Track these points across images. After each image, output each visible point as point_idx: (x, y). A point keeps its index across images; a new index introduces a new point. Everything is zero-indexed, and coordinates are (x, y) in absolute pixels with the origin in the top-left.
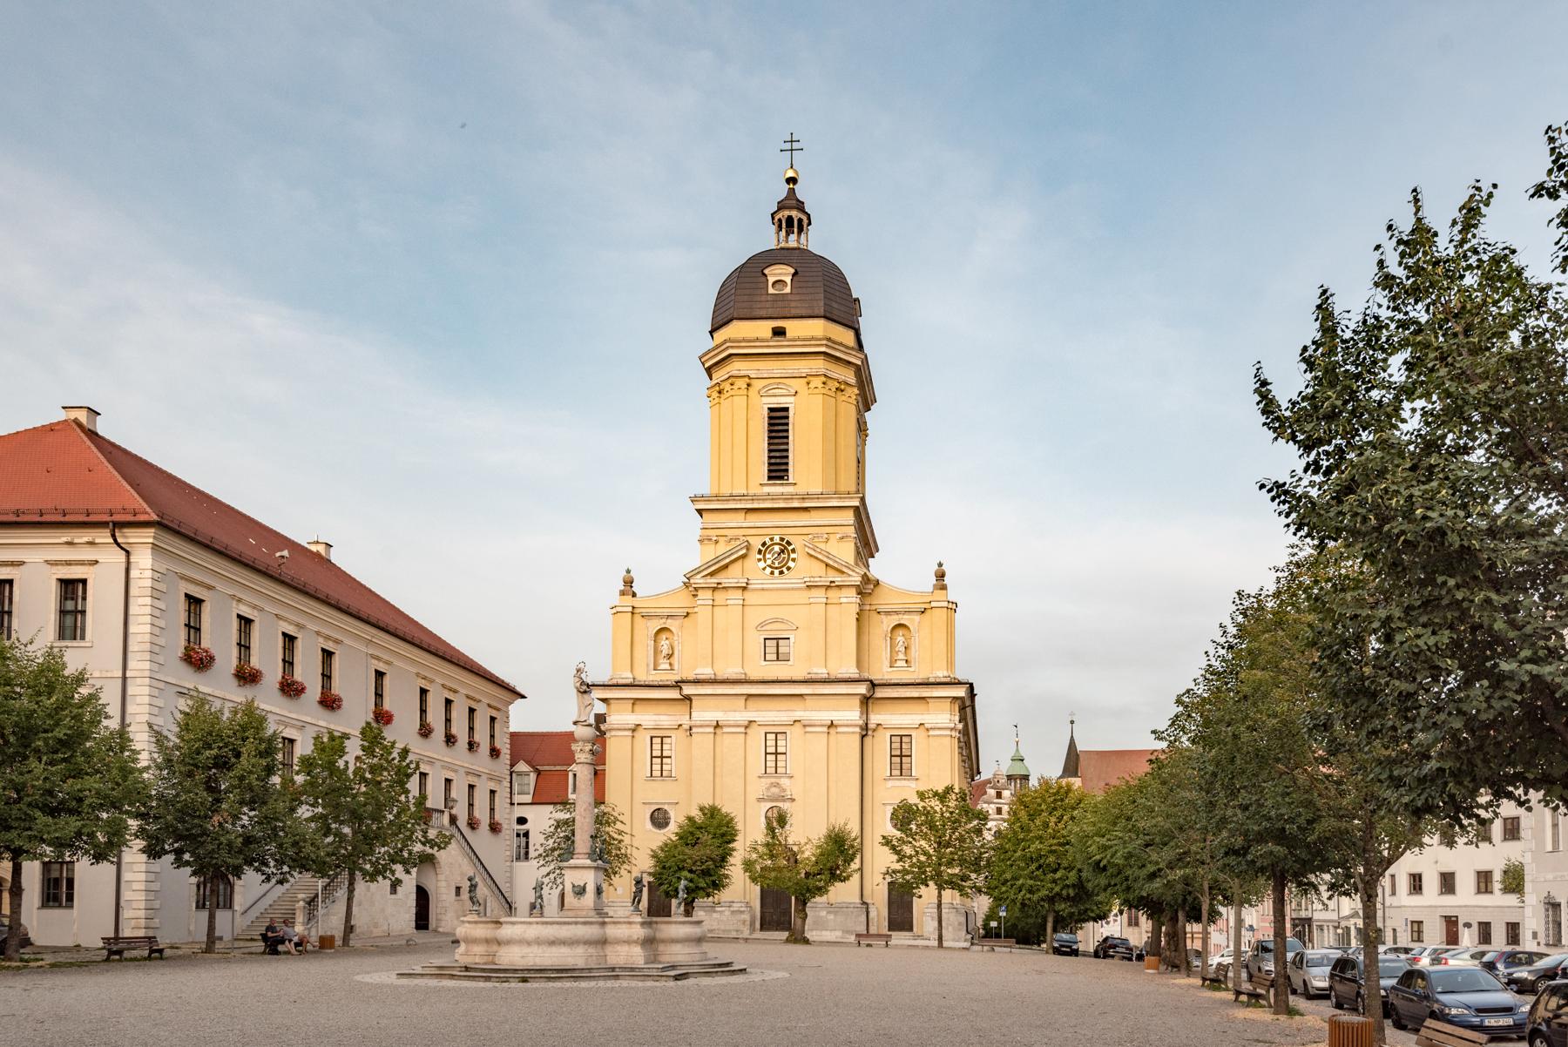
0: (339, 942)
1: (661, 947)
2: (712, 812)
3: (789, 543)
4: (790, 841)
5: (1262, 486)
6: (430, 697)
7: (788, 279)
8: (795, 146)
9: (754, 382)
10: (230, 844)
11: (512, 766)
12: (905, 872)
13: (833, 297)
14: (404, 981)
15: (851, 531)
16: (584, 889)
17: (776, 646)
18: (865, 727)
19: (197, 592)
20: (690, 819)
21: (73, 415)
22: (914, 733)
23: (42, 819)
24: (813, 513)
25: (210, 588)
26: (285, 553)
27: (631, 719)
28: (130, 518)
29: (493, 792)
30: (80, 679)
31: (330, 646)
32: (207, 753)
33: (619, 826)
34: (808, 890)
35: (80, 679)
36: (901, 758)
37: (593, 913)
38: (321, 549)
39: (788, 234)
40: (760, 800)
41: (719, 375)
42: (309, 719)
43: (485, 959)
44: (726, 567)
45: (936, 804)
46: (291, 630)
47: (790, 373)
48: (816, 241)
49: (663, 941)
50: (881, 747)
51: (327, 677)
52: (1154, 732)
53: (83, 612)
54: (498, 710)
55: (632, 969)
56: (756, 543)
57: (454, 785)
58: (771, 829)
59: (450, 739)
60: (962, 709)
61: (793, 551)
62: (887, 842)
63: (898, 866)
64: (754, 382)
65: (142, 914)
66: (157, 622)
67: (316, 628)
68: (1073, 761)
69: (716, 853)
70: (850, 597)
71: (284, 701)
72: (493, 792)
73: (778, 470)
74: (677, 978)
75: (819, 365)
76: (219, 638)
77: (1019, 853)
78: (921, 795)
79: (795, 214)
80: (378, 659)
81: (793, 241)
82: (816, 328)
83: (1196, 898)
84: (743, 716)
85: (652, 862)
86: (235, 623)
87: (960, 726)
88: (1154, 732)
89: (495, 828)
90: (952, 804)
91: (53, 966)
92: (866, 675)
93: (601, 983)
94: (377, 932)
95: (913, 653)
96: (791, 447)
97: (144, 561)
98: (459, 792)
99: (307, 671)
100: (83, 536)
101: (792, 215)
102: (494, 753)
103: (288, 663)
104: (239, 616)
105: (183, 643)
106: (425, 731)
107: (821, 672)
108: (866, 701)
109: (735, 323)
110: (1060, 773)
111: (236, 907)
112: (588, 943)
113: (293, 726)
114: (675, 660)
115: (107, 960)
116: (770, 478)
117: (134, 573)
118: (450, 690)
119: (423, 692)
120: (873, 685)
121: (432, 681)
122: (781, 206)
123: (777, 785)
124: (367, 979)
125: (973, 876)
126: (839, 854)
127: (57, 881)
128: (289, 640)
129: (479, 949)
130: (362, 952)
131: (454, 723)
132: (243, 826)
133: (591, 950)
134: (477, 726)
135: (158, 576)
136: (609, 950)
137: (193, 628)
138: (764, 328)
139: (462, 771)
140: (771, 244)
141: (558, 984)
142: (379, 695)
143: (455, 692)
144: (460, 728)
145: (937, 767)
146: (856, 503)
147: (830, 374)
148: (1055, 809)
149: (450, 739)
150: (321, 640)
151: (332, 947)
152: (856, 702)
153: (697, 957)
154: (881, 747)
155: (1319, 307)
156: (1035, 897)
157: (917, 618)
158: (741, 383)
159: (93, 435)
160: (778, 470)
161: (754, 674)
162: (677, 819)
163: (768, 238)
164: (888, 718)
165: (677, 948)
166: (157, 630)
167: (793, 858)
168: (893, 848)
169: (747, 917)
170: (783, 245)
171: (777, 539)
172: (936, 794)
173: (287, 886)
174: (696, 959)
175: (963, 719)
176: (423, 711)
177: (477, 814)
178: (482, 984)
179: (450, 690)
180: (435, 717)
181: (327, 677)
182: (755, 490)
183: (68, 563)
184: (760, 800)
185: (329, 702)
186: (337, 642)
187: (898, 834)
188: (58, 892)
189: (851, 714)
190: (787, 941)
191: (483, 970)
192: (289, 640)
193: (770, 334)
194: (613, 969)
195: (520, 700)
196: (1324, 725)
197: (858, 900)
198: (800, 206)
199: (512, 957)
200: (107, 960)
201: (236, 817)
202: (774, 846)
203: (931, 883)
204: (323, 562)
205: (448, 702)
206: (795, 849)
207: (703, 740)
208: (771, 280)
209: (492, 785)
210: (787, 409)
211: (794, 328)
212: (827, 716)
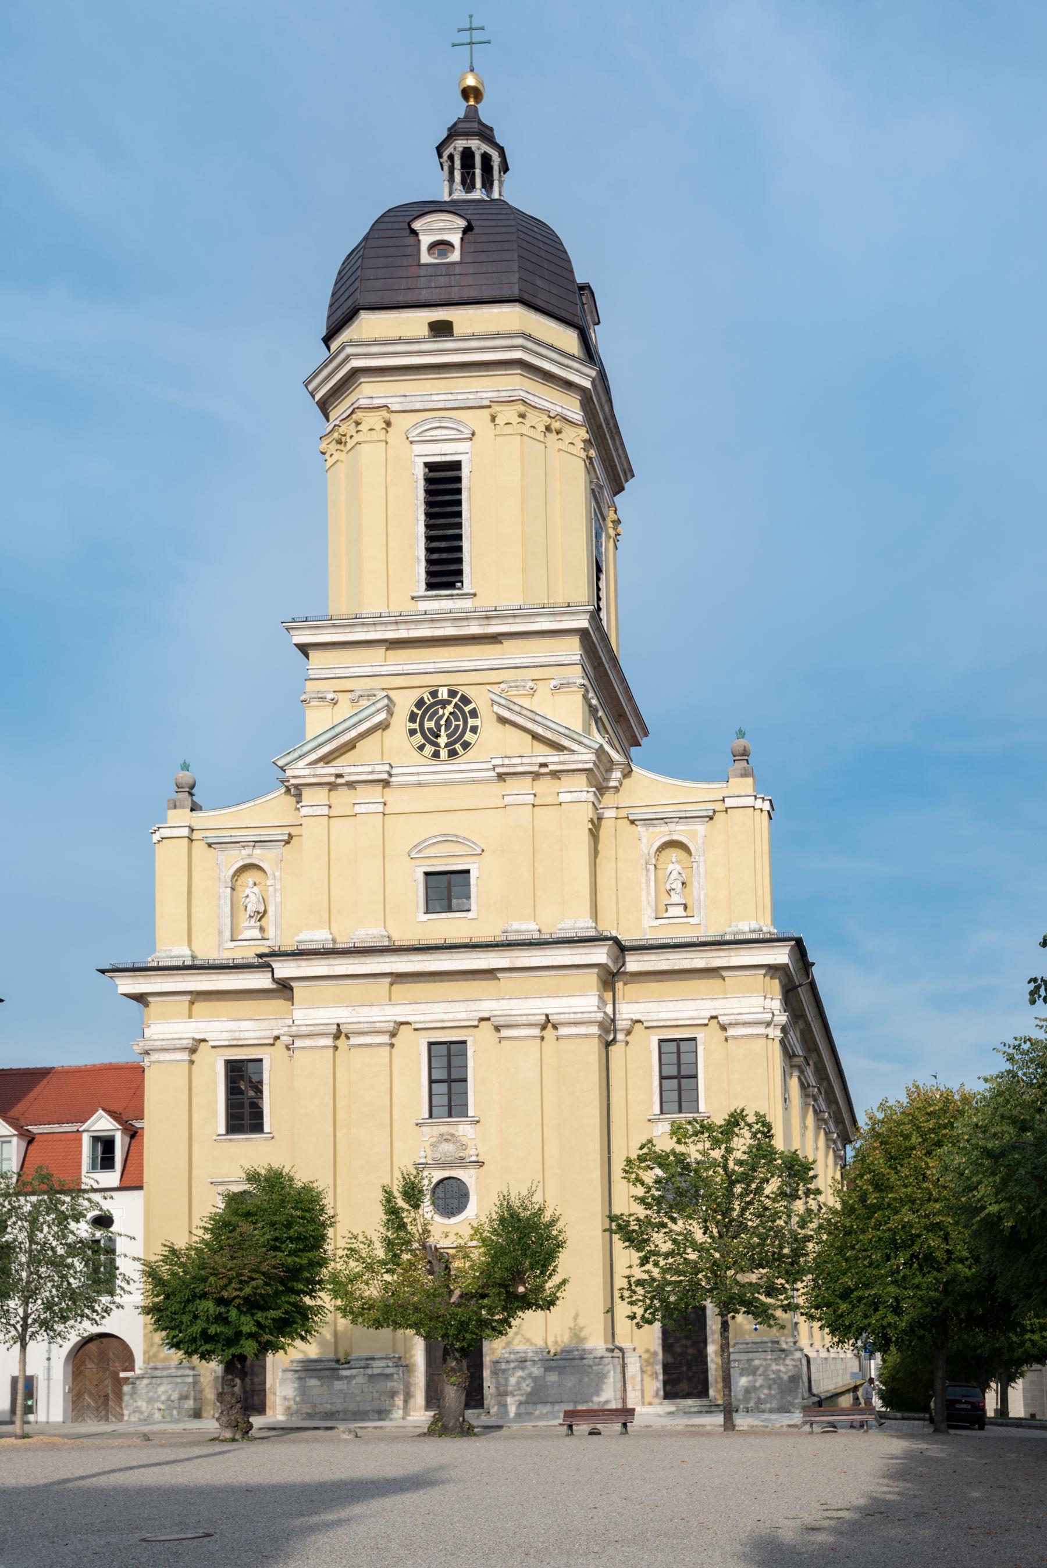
7: (455, 239)
8: (477, 36)
9: (394, 418)
13: (536, 270)
15: (577, 675)
17: (446, 889)
22: (700, 1035)
24: (507, 644)
36: (678, 1073)
47: (461, 399)
50: (640, 1066)
56: (405, 703)
61: (474, 714)
64: (394, 418)
70: (577, 792)
73: (444, 568)
75: (514, 383)
82: (511, 317)
84: (385, 1014)
95: (699, 891)
96: (466, 531)
107: (526, 927)
114: (269, 922)
116: (430, 586)
120: (621, 949)
126: (523, 1256)
138: (415, 322)
146: (583, 623)
148: (939, 1144)
152: (592, 978)
157: (700, 828)
160: (444, 568)
164: (634, 1005)
171: (443, 694)
182: (401, 604)
189: (582, 1001)
193: (425, 331)
198: (486, 134)
208: (426, 240)
210: (457, 465)
212: (537, 1007)
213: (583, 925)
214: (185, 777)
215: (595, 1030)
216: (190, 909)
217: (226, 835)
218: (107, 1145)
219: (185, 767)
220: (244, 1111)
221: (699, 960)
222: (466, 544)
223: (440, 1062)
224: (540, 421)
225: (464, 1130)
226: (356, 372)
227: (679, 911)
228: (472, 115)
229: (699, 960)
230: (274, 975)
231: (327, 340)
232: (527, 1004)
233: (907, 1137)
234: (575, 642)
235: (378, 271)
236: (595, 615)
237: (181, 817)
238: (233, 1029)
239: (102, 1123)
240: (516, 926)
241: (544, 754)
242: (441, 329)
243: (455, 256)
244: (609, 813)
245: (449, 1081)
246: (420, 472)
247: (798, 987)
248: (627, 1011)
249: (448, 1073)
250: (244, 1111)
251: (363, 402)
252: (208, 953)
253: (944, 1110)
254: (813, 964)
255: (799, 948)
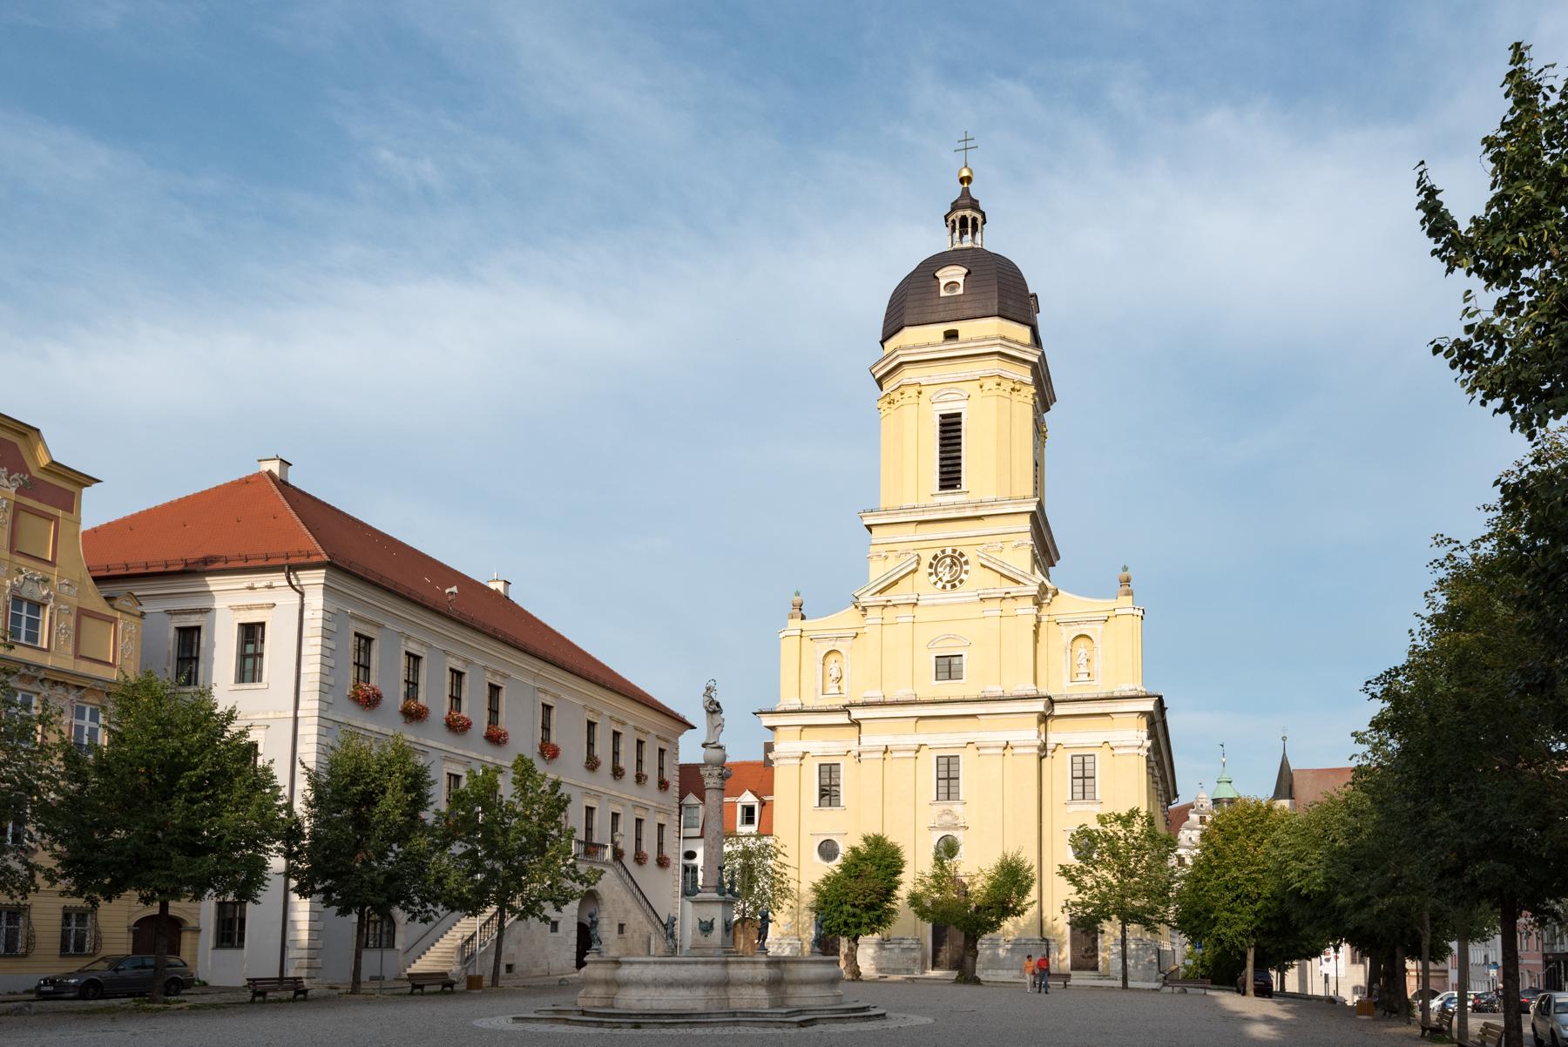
0: (487, 982)
1: (790, 990)
2: (877, 842)
3: (961, 555)
4: (961, 872)
5: (1438, 349)
6: (598, 731)
7: (961, 280)
9: (923, 389)
10: (372, 882)
11: (681, 798)
12: (1085, 905)
13: (1005, 290)
14: (519, 1026)
15: (1028, 539)
16: (711, 924)
17: (948, 667)
18: (1043, 749)
19: (366, 631)
20: (854, 850)
21: (266, 467)
22: (1097, 752)
23: (178, 858)
24: (987, 520)
25: (380, 626)
26: (454, 589)
27: (799, 747)
28: (303, 560)
29: (661, 826)
30: (230, 716)
31: (497, 681)
32: (354, 790)
33: (781, 858)
34: (979, 925)
35: (230, 716)
36: (1084, 779)
37: (720, 952)
38: (499, 586)
39: (961, 236)
40: (931, 828)
41: (889, 385)
42: (474, 755)
43: (604, 1002)
44: (896, 583)
45: (1118, 828)
46: (459, 666)
48: (991, 240)
49: (792, 983)
50: (1059, 770)
51: (494, 712)
52: (1354, 734)
53: (261, 655)
54: (667, 741)
55: (754, 1014)
56: (927, 558)
57: (621, 819)
58: (939, 860)
59: (617, 772)
60: (1151, 725)
61: (966, 563)
62: (1065, 872)
63: (1076, 899)
64: (923, 389)
65: (305, 953)
66: (327, 661)
67: (484, 662)
68: (1286, 784)
69: (880, 885)
70: (1028, 607)
71: (450, 737)
72: (661, 826)
73: (950, 477)
74: (801, 1024)
75: (994, 365)
76: (387, 677)
77: (1213, 882)
78: (1102, 820)
79: (968, 213)
80: (545, 692)
81: (967, 242)
83: (1415, 932)
84: (913, 740)
85: (813, 896)
86: (403, 661)
87: (1148, 743)
88: (1354, 734)
89: (662, 862)
90: (1137, 828)
91: (191, 1008)
92: (1043, 691)
93: (718, 1031)
94: (536, 971)
95: (1097, 665)
96: (963, 454)
97: (316, 601)
98: (626, 827)
99: (474, 707)
100: (261, 580)
101: (966, 215)
102: (663, 785)
103: (456, 699)
104: (407, 653)
105: (351, 681)
106: (592, 764)
107: (996, 690)
108: (1044, 718)
109: (906, 330)
110: (1271, 794)
111: (398, 946)
112: (709, 984)
113: (458, 762)
114: (843, 682)
115: (411, 993)
116: (942, 487)
117: (306, 615)
118: (618, 722)
119: (591, 725)
120: (1052, 702)
121: (600, 714)
122: (955, 207)
123: (949, 812)
124: (483, 1023)
125: (1162, 908)
126: (1012, 883)
127: (231, 922)
128: (457, 675)
129: (598, 991)
130: (511, 993)
131: (622, 756)
132: (390, 863)
133: (713, 993)
134: (646, 757)
135: (329, 616)
136: (732, 992)
137: (363, 666)
138: (936, 332)
139: (629, 804)
140: (947, 247)
141: (672, 1031)
142: (546, 728)
143: (623, 724)
144: (627, 761)
145: (1124, 788)
146: (1033, 508)
147: (1004, 374)
148: (1254, 832)
149: (617, 772)
150: (488, 675)
151: (479, 987)
152: (1034, 719)
153: (831, 1001)
154: (1059, 770)
155: (1511, 75)
156: (1230, 933)
157: (1099, 627)
158: (912, 391)
159: (283, 485)
160: (950, 477)
161: (924, 695)
162: (843, 850)
163: (942, 240)
164: (1058, 734)
165: (807, 991)
166: (327, 670)
167: (963, 889)
168: (1072, 880)
169: (917, 955)
170: (957, 246)
171: (948, 551)
172: (1118, 817)
173: (430, 924)
174: (830, 1002)
175: (1152, 735)
176: (590, 744)
177: (644, 848)
178: (592, 1030)
179: (618, 722)
180: (603, 750)
181: (494, 712)
182: (926, 500)
183: (249, 608)
184: (931, 828)
185: (495, 738)
186: (504, 676)
187: (1077, 863)
188: (230, 932)
189: (1028, 734)
190: (957, 981)
191: (598, 1014)
192: (457, 675)
193: (941, 337)
194: (734, 1014)
195: (690, 731)
196: (1542, 684)
197: (1037, 937)
198: (974, 205)
199: (631, 999)
200: (253, 1001)
201: (381, 856)
202: (944, 877)
203: (1114, 917)
204: (502, 600)
205: (616, 735)
206: (966, 880)
207: (872, 762)
208: (943, 282)
209: (661, 819)
210: (959, 415)
211: (965, 328)
212: (1002, 738)
213: (1029, 689)
214: (797, 600)
215: (1035, 750)
216: (800, 679)
217: (820, 634)
218: (749, 811)
219: (798, 594)
220: (828, 794)
221: (1098, 707)
222: (963, 461)
223: (943, 768)
224: (1008, 385)
225: (957, 808)
226: (901, 364)
227: (1085, 677)
228: (966, 192)
229: (1098, 707)
230: (850, 716)
231: (882, 343)
232: (990, 733)
233: (1235, 828)
234: (1027, 517)
235: (912, 301)
236: (1040, 505)
237: (796, 624)
238: (824, 746)
239: (748, 798)
240: (990, 688)
241: (1009, 586)
242: (951, 335)
243: (960, 291)
244: (1044, 619)
245: (949, 779)
246: (937, 421)
247: (1157, 723)
248: (1053, 739)
249: (948, 777)
250: (828, 794)
251: (906, 381)
252: (810, 703)
253: (1256, 813)
254: (1450, 270)
255: (1160, 701)
